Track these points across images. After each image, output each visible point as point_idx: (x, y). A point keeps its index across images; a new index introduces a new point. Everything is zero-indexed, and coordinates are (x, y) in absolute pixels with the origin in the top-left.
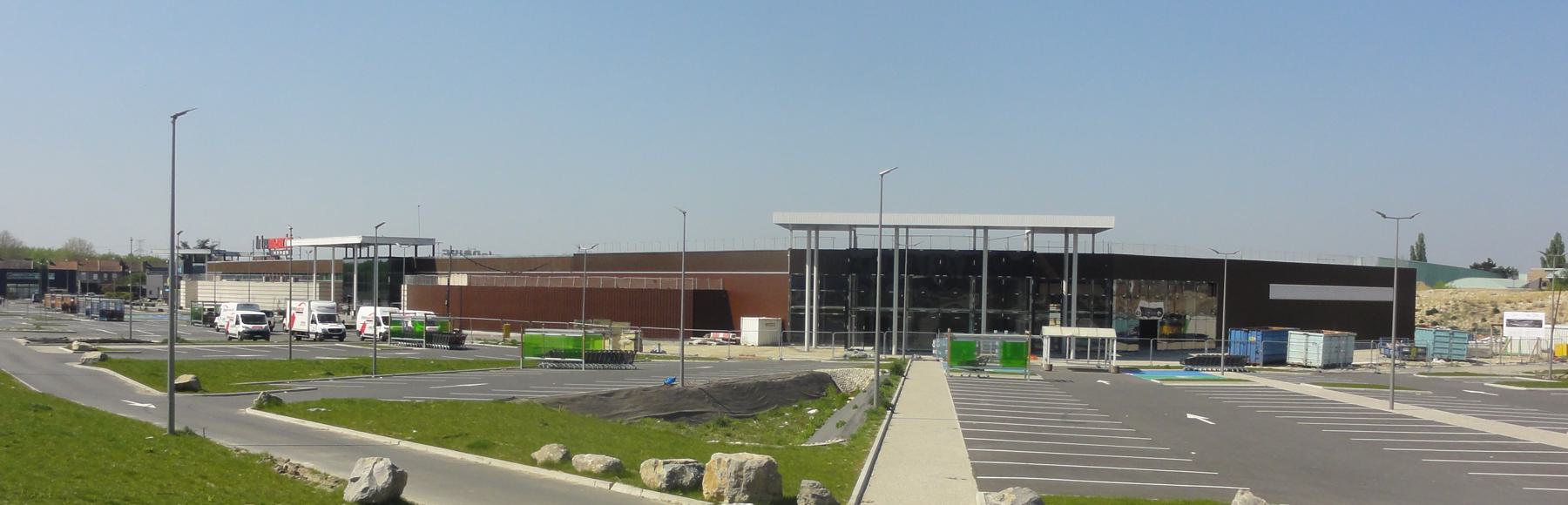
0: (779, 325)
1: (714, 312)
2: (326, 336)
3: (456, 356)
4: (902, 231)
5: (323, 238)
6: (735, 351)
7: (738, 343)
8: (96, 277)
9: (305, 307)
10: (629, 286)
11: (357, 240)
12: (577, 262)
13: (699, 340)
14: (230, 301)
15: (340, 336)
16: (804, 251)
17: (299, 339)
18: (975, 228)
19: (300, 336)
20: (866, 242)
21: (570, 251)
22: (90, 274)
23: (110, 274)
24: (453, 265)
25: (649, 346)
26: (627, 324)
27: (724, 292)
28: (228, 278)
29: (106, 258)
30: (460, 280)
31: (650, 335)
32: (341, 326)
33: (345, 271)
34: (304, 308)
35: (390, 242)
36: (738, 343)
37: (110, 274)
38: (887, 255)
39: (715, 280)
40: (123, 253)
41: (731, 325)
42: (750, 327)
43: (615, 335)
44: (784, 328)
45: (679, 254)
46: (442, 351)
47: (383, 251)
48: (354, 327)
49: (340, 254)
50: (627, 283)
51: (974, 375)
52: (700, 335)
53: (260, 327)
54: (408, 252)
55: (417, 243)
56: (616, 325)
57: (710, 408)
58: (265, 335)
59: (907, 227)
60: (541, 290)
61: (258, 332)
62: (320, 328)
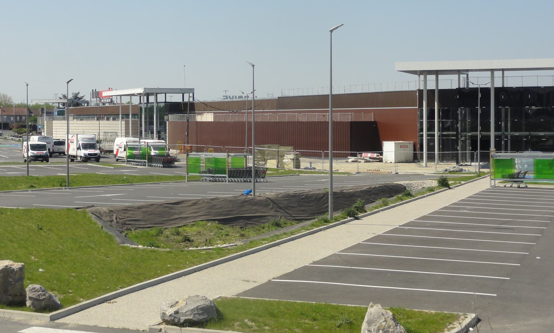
0: (411, 147)
1: (364, 137)
2: (87, 159)
3: (168, 172)
4: (498, 74)
5: (126, 90)
6: (376, 165)
7: (381, 161)
8: (12, 119)
9: (75, 138)
10: (304, 119)
11: (141, 91)
12: (284, 103)
13: (353, 159)
14: (74, 134)
15: (96, 158)
16: (434, 90)
17: (72, 160)
18: (492, 71)
19: (73, 158)
20: (479, 81)
21: (276, 95)
22: (9, 116)
23: (21, 117)
24: (208, 106)
25: (305, 163)
26: (290, 148)
27: (375, 123)
28: (77, 118)
29: (19, 106)
30: (208, 117)
31: (304, 155)
32: (97, 152)
33: (137, 112)
34: (121, 140)
35: (166, 92)
36: (381, 161)
37: (21, 117)
38: (486, 91)
39: (367, 115)
40: (42, 103)
41: (379, 149)
42: (389, 148)
43: (280, 157)
44: (415, 150)
45: (326, 96)
46: (158, 170)
47: (161, 98)
48: (112, 151)
49: (125, 100)
50: (303, 118)
51: (515, 185)
52: (355, 155)
53: (97, 153)
54: (176, 98)
55: (183, 92)
56: (282, 149)
57: (272, 213)
58: (96, 158)
59: (503, 70)
60: (235, 123)
61: (40, 156)
62: (83, 153)
